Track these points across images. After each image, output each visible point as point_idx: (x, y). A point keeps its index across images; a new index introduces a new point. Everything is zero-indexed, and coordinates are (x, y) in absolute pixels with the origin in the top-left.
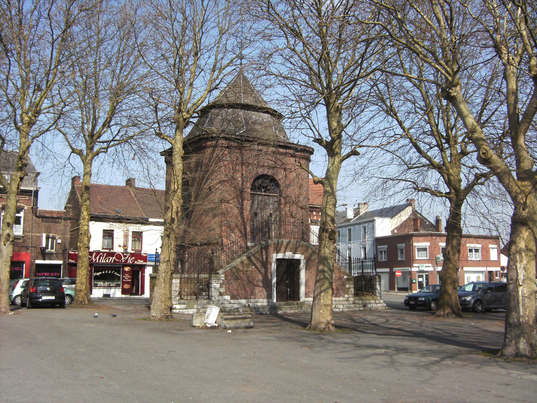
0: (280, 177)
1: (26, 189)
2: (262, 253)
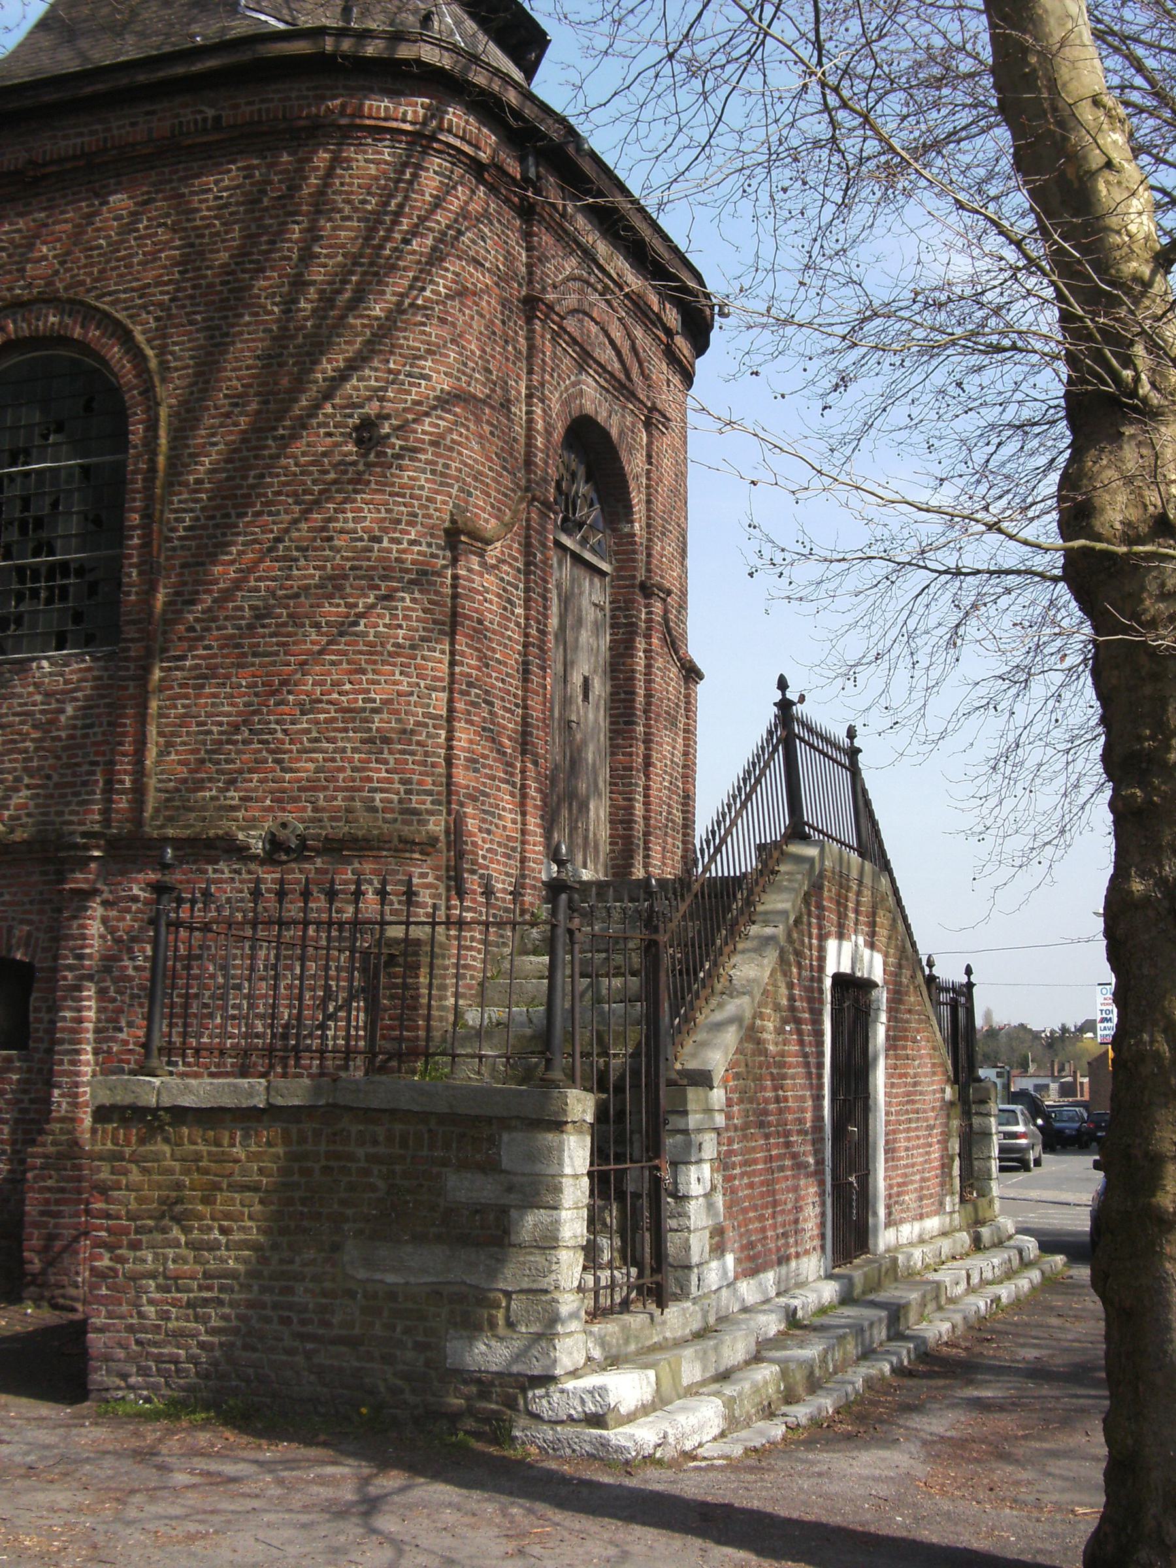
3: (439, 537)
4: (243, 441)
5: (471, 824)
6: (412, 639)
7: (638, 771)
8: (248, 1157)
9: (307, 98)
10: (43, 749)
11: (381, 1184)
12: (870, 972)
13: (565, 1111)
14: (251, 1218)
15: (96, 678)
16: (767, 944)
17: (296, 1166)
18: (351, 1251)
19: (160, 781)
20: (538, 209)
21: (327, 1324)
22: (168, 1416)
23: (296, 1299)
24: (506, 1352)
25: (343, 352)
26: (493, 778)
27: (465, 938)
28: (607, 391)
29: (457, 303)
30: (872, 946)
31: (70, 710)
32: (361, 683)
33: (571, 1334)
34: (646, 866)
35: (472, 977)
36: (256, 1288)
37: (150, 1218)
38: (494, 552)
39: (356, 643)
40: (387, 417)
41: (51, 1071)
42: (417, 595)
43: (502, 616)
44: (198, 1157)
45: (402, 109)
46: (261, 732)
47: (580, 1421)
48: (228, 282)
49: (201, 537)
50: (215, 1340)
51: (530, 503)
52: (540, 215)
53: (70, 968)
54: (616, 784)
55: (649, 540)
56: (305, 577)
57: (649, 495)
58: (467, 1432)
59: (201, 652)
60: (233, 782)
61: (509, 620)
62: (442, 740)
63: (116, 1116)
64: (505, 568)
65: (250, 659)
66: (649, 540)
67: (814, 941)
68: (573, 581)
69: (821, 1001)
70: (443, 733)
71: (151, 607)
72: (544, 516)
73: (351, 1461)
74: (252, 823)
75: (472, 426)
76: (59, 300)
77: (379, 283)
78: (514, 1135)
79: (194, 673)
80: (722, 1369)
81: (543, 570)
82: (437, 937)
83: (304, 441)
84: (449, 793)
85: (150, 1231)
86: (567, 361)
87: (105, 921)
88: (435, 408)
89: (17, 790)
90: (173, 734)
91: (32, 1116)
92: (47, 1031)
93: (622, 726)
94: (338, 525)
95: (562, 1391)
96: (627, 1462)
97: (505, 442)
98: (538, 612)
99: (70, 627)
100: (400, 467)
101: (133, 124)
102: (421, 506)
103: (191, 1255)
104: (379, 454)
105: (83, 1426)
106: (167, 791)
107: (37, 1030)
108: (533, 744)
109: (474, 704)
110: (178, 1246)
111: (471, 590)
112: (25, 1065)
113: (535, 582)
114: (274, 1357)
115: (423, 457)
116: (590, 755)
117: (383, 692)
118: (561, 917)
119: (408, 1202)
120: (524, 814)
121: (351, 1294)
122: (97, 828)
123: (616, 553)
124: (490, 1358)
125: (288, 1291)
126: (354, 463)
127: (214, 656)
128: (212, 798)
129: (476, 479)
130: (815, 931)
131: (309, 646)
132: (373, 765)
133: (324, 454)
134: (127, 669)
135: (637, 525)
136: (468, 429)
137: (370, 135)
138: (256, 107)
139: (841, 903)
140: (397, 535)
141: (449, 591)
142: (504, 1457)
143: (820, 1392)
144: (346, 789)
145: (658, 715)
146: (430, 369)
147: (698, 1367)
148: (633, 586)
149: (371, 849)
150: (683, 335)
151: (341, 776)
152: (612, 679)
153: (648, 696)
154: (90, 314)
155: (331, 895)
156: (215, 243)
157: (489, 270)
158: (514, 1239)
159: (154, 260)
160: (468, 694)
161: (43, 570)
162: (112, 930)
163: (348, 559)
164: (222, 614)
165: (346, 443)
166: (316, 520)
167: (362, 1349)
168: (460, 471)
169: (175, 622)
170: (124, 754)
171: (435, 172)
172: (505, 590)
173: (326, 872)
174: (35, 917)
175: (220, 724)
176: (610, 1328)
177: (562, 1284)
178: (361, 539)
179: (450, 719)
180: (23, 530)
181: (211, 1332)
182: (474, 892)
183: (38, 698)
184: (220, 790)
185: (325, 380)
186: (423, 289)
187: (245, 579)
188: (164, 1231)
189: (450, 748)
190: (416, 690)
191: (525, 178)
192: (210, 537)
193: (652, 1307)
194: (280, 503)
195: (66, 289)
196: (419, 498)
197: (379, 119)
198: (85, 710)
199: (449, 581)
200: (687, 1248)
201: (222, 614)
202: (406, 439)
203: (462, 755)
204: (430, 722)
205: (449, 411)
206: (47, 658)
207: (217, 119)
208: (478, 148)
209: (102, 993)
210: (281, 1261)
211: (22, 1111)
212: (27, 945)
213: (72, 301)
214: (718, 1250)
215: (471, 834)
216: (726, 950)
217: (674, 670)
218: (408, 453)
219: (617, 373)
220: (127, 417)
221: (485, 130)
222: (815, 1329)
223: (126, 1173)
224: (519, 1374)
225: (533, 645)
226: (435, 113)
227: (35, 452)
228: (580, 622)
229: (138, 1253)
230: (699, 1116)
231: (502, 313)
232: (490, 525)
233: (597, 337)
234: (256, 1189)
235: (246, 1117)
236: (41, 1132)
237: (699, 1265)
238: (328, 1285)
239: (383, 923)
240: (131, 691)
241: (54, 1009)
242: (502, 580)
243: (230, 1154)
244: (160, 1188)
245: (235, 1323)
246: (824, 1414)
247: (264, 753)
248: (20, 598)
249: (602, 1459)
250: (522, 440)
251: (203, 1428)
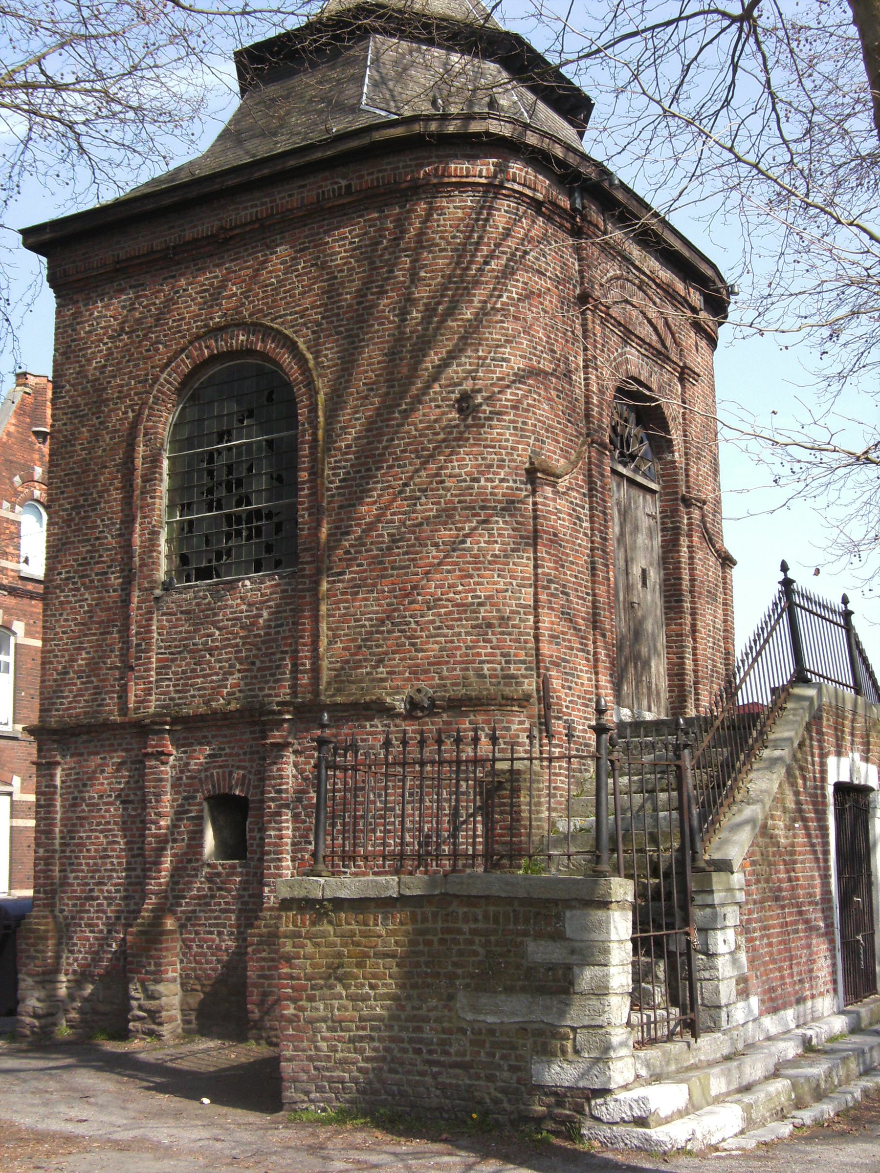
3: (521, 475)
4: (378, 415)
5: (556, 683)
6: (505, 550)
7: (687, 636)
8: (387, 933)
9: (411, 166)
10: (249, 643)
11: (481, 951)
12: (866, 780)
13: (610, 894)
14: (391, 977)
15: (283, 591)
16: (775, 764)
17: (421, 939)
18: (462, 1000)
19: (331, 663)
20: (585, 230)
21: (446, 1053)
22: (338, 1121)
23: (424, 1035)
24: (574, 1072)
25: (445, 346)
26: (572, 649)
27: (555, 767)
28: (648, 357)
29: (526, 305)
30: (867, 760)
31: (265, 614)
32: (470, 584)
33: (621, 1058)
34: (697, 706)
35: (561, 796)
36: (396, 1028)
37: (321, 978)
38: (563, 483)
39: (465, 556)
40: (479, 391)
41: (262, 874)
42: (507, 519)
43: (573, 530)
44: (352, 934)
45: (478, 168)
46: (400, 624)
47: (630, 1122)
48: (362, 302)
49: (352, 486)
50: (369, 1065)
51: (590, 445)
52: (586, 234)
53: (273, 800)
54: (671, 647)
55: (687, 464)
56: (426, 510)
57: (685, 431)
58: (548, 1131)
59: (355, 568)
60: (381, 661)
61: (578, 532)
62: (531, 623)
63: (295, 906)
64: (575, 494)
65: (390, 572)
66: (687, 464)
67: (817, 759)
68: (629, 499)
69: (824, 804)
70: (531, 618)
71: (318, 538)
72: (601, 453)
73: (463, 1153)
74: (397, 690)
75: (542, 393)
76: (245, 323)
77: (468, 294)
78: (574, 912)
79: (351, 584)
80: (745, 1083)
81: (602, 493)
82: (534, 767)
83: (421, 412)
84: (538, 662)
85: (322, 988)
86: (615, 338)
87: (296, 765)
88: (514, 382)
89: (232, 674)
90: (338, 628)
91: (251, 907)
92: (259, 846)
93: (674, 604)
94: (448, 471)
95: (616, 1100)
96: (665, 1153)
97: (569, 402)
98: (600, 524)
99: (264, 555)
100: (491, 427)
101: (290, 196)
102: (507, 454)
103: (350, 1004)
104: (474, 419)
105: (277, 1129)
106: (335, 670)
107: (252, 845)
108: (601, 622)
109: (552, 595)
110: (341, 998)
111: (548, 512)
112: (244, 871)
113: (597, 503)
114: (410, 1078)
115: (506, 418)
116: (649, 626)
117: (486, 590)
118: (603, 752)
119: (500, 963)
120: (597, 673)
121: (463, 1031)
122: (288, 698)
123: (663, 476)
124: (563, 1077)
125: (419, 1029)
126: (457, 426)
127: (365, 571)
128: (367, 674)
129: (547, 431)
130: (816, 751)
131: (431, 560)
132: (482, 644)
133: (436, 421)
134: (305, 583)
135: (677, 454)
136: (540, 395)
137: (457, 188)
138: (375, 176)
139: (838, 730)
140: (491, 476)
141: (531, 514)
142: (575, 1150)
143: (825, 1100)
144: (463, 662)
145: (701, 593)
146: (509, 354)
147: (723, 1080)
148: (676, 499)
149: (482, 705)
150: (706, 310)
151: (458, 653)
152: (665, 569)
153: (692, 580)
154: (268, 332)
155: (458, 741)
156: (351, 275)
157: (550, 278)
158: (577, 989)
159: (310, 291)
160: (549, 588)
161: (244, 516)
162: (301, 772)
163: (456, 496)
164: (368, 541)
165: (450, 412)
166: (431, 469)
167: (472, 1071)
168: (535, 426)
169: (336, 548)
170: (305, 645)
171: (506, 211)
172: (574, 510)
173: (450, 723)
174: (247, 764)
175: (371, 619)
176: (653, 1053)
177: (613, 1021)
178: (465, 481)
179: (536, 607)
180: (229, 489)
181: (366, 1060)
182: (560, 733)
183: (244, 607)
184: (373, 667)
185: (433, 367)
186: (500, 296)
187: (384, 515)
188: (331, 987)
189: (537, 628)
190: (510, 587)
191: (574, 209)
192: (358, 485)
193: (688, 1037)
194: (406, 458)
195: (250, 315)
196: (506, 448)
197: (462, 177)
198: (276, 613)
199: (530, 507)
200: (718, 993)
201: (368, 541)
202: (494, 406)
203: (546, 633)
204: (522, 610)
205: (524, 383)
206: (249, 578)
207: (348, 187)
208: (535, 190)
209: (296, 817)
210: (413, 1008)
211: (244, 903)
212: (243, 784)
213: (254, 324)
214: (744, 993)
215: (555, 691)
216: (744, 769)
217: (713, 559)
218: (496, 417)
219: (654, 344)
220: (297, 403)
221: (540, 177)
222: (826, 1052)
223: (303, 946)
224: (585, 1088)
225: (598, 549)
226: (501, 168)
227: (234, 432)
228: (636, 529)
229: (314, 1004)
230: (722, 894)
231: (562, 308)
232: (559, 463)
233: (637, 318)
234: (393, 956)
235: (385, 904)
236: (257, 918)
237: (727, 1006)
238: (446, 1025)
239: (494, 760)
240: (308, 599)
241: (263, 830)
242: (571, 503)
243: (374, 931)
244: (327, 956)
245: (382, 1053)
246: (826, 1116)
247: (403, 639)
248: (229, 537)
249: (646, 1151)
250: (582, 400)
251: (361, 1130)
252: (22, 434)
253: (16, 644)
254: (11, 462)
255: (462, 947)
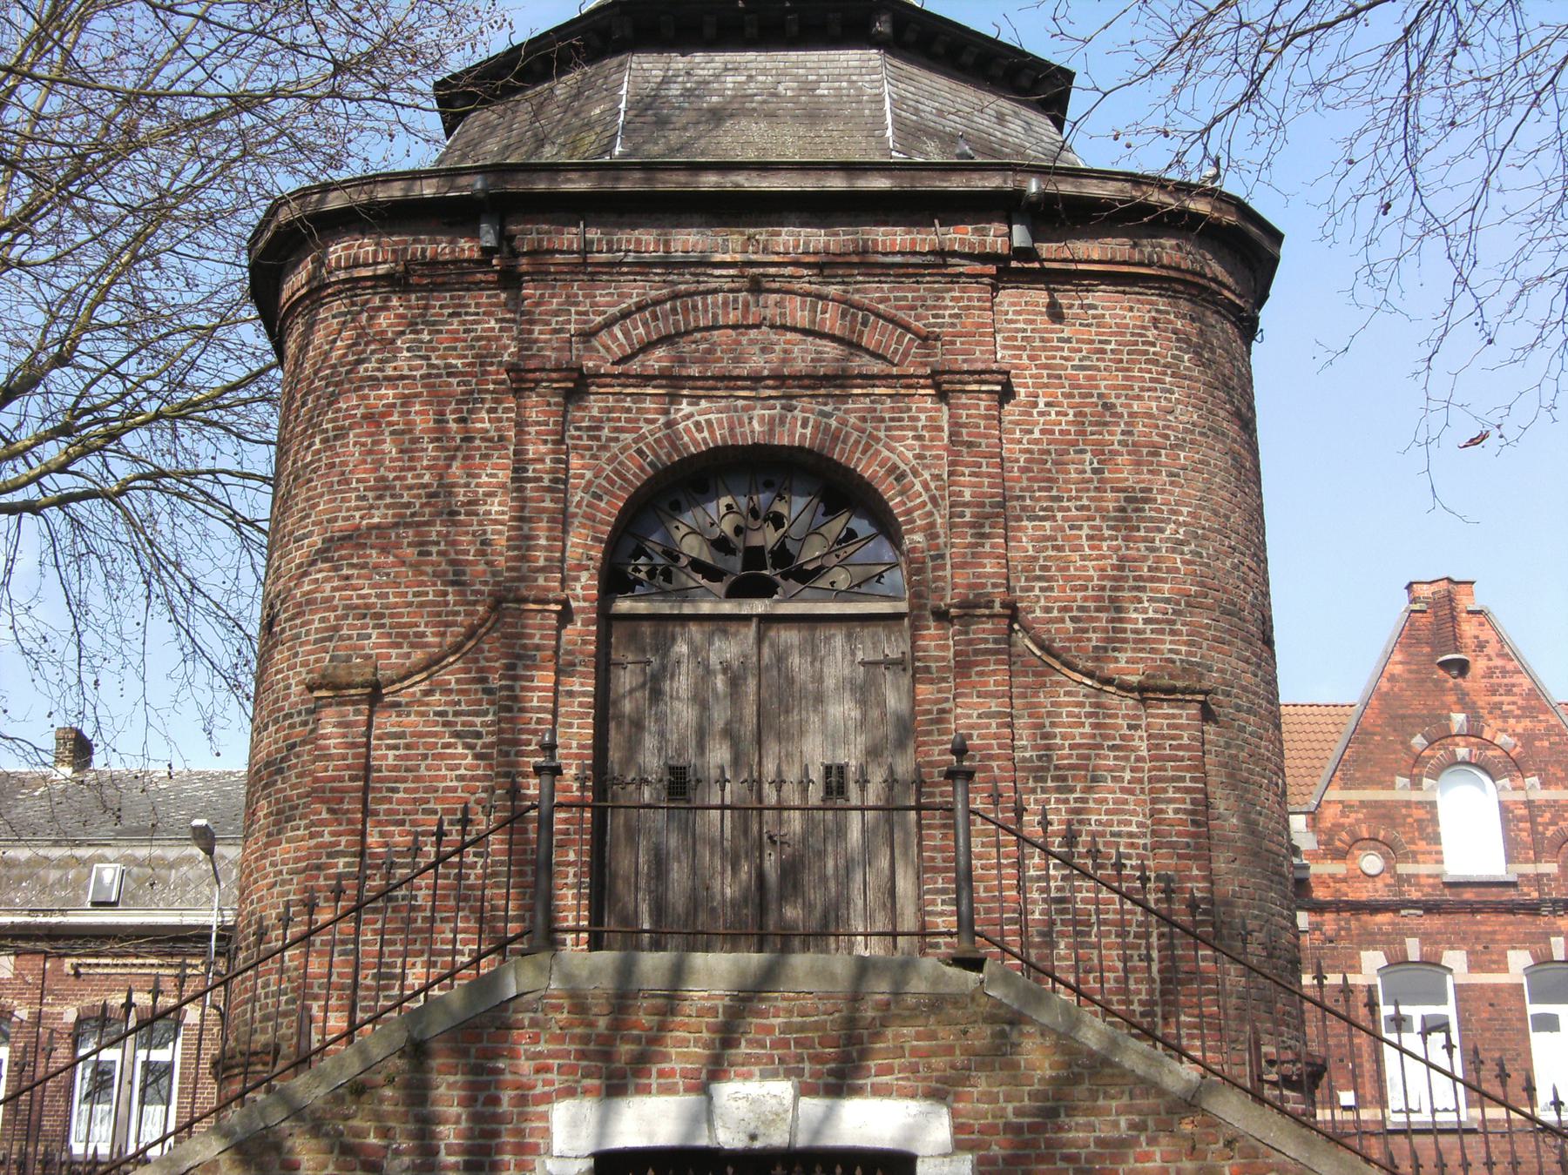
0: (905, 451)
1: (190, 919)
2: (418, 1094)
252: (1418, 672)
253: (1455, 986)
254: (1403, 717)
255: (968, 237)
